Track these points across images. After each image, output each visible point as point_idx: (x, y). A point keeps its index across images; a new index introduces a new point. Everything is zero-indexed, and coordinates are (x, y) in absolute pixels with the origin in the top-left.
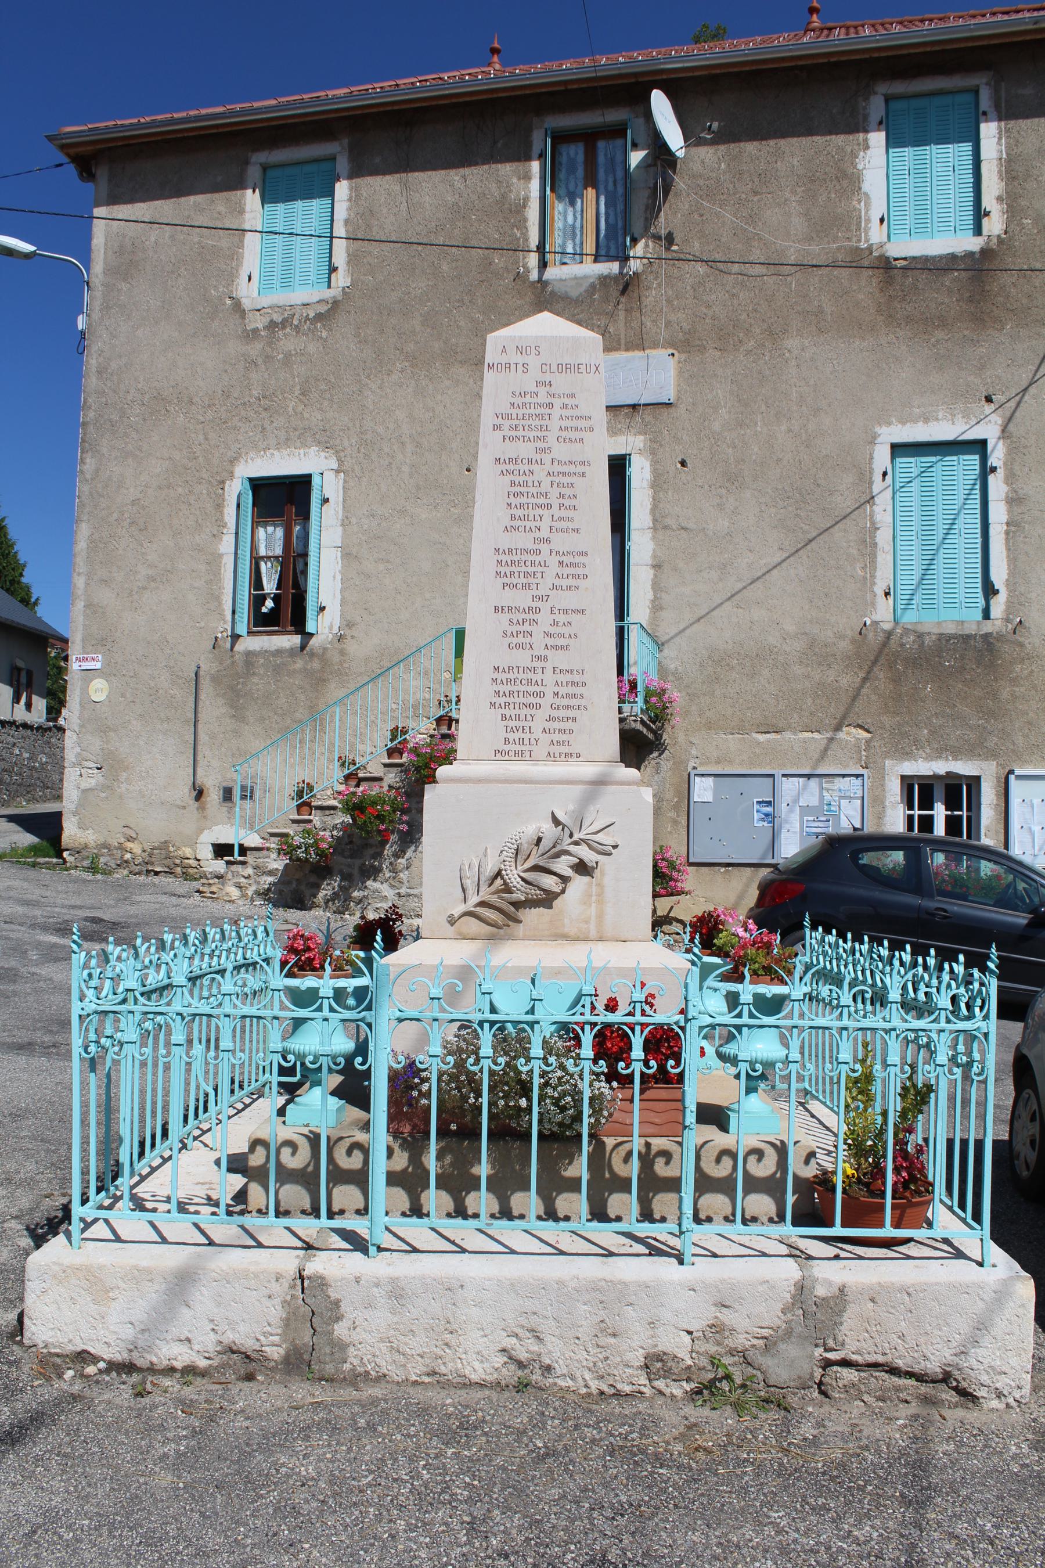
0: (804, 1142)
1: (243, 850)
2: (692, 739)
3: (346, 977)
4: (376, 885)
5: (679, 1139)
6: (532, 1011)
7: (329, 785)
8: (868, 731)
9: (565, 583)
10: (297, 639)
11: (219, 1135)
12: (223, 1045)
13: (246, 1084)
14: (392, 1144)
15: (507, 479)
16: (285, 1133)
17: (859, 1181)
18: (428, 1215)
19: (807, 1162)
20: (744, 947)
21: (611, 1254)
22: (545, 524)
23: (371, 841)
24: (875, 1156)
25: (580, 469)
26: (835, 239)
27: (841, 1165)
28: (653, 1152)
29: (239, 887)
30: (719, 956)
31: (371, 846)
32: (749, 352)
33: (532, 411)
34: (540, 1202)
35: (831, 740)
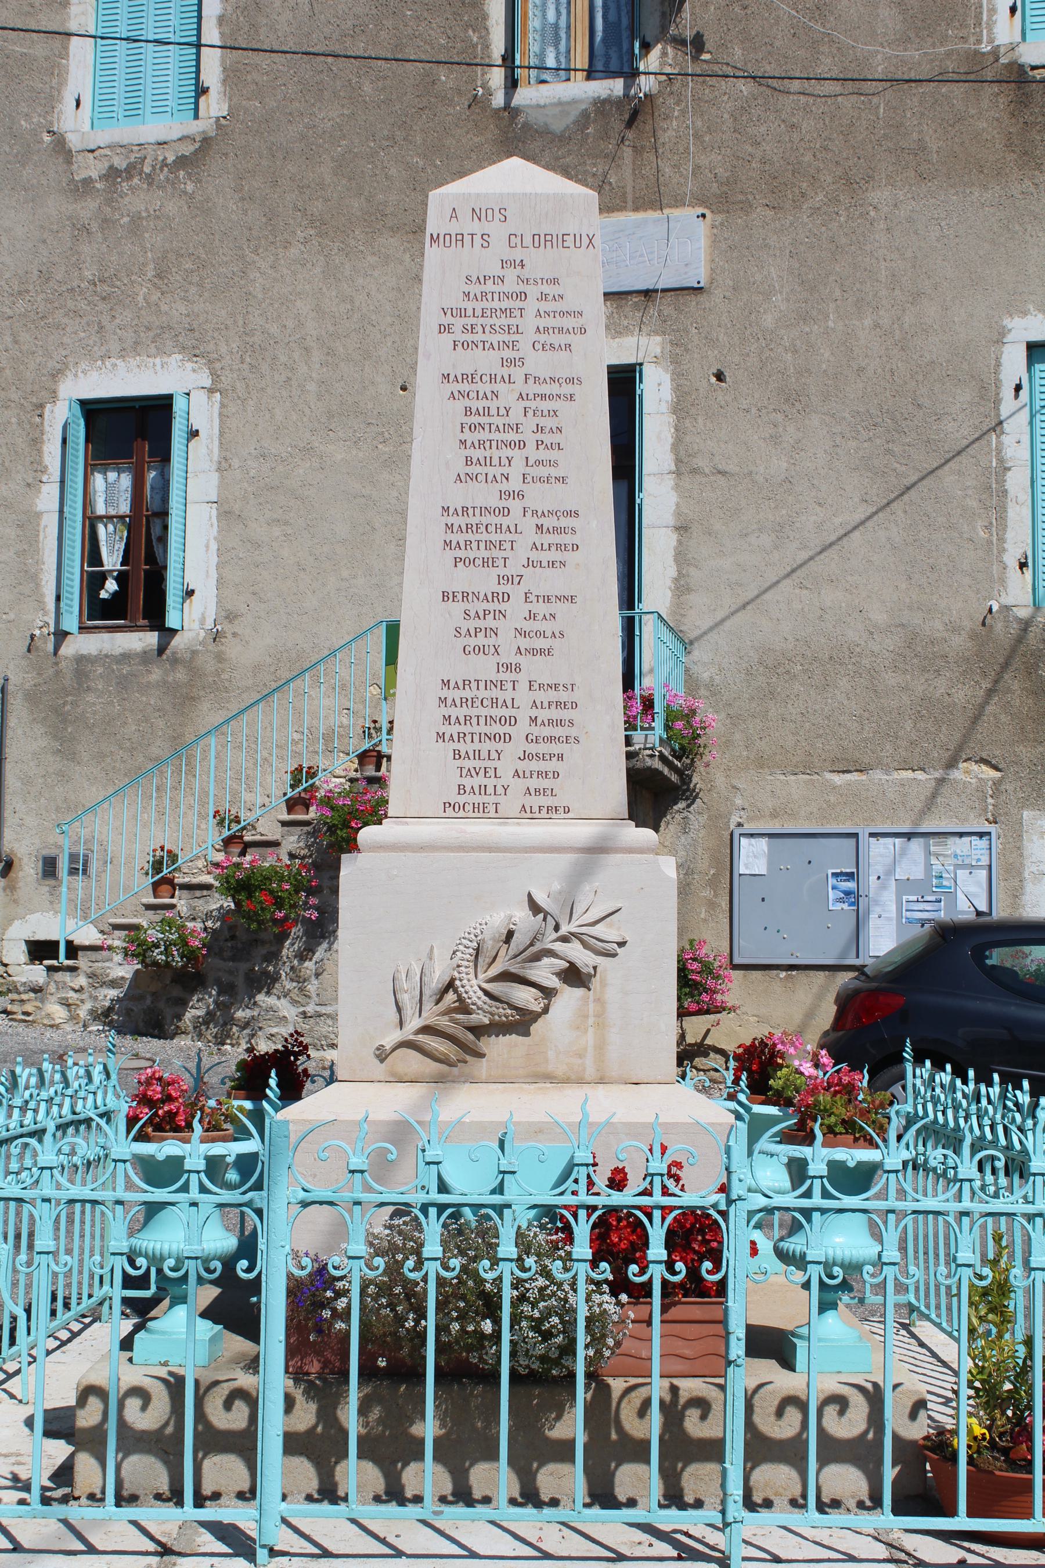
0: (908, 1385)
1: (73, 950)
2: (735, 782)
3: (224, 1139)
4: (271, 1001)
5: (721, 1381)
6: (499, 1189)
7: (200, 851)
8: (996, 768)
9: (545, 556)
10: (151, 638)
11: (32, 1380)
12: (40, 1244)
13: (74, 1301)
14: (292, 1390)
15: (460, 404)
16: (132, 1376)
17: (993, 1445)
18: (345, 1499)
19: (913, 1415)
20: (813, 1091)
21: (621, 1557)
22: (516, 471)
23: (263, 936)
24: (1016, 1407)
25: (567, 389)
26: (944, 39)
27: (964, 1419)
28: (682, 1401)
29: (66, 1004)
30: (774, 1104)
31: (263, 943)
32: (815, 210)
33: (496, 304)
34: (514, 1477)
35: (941, 781)
